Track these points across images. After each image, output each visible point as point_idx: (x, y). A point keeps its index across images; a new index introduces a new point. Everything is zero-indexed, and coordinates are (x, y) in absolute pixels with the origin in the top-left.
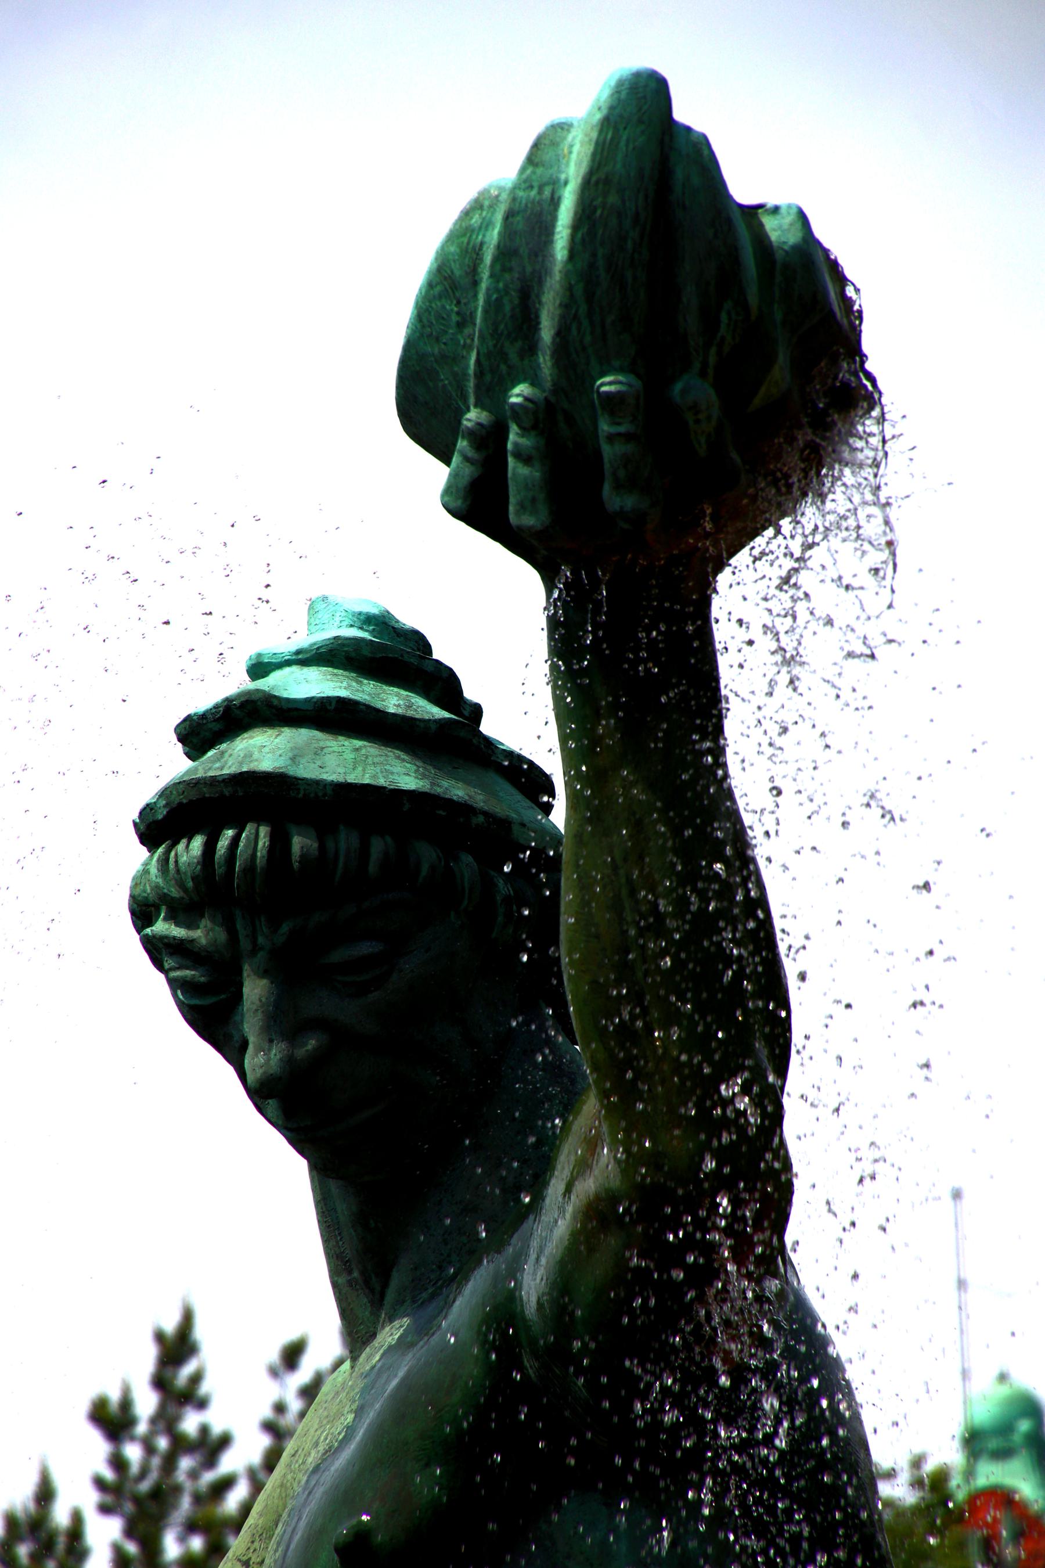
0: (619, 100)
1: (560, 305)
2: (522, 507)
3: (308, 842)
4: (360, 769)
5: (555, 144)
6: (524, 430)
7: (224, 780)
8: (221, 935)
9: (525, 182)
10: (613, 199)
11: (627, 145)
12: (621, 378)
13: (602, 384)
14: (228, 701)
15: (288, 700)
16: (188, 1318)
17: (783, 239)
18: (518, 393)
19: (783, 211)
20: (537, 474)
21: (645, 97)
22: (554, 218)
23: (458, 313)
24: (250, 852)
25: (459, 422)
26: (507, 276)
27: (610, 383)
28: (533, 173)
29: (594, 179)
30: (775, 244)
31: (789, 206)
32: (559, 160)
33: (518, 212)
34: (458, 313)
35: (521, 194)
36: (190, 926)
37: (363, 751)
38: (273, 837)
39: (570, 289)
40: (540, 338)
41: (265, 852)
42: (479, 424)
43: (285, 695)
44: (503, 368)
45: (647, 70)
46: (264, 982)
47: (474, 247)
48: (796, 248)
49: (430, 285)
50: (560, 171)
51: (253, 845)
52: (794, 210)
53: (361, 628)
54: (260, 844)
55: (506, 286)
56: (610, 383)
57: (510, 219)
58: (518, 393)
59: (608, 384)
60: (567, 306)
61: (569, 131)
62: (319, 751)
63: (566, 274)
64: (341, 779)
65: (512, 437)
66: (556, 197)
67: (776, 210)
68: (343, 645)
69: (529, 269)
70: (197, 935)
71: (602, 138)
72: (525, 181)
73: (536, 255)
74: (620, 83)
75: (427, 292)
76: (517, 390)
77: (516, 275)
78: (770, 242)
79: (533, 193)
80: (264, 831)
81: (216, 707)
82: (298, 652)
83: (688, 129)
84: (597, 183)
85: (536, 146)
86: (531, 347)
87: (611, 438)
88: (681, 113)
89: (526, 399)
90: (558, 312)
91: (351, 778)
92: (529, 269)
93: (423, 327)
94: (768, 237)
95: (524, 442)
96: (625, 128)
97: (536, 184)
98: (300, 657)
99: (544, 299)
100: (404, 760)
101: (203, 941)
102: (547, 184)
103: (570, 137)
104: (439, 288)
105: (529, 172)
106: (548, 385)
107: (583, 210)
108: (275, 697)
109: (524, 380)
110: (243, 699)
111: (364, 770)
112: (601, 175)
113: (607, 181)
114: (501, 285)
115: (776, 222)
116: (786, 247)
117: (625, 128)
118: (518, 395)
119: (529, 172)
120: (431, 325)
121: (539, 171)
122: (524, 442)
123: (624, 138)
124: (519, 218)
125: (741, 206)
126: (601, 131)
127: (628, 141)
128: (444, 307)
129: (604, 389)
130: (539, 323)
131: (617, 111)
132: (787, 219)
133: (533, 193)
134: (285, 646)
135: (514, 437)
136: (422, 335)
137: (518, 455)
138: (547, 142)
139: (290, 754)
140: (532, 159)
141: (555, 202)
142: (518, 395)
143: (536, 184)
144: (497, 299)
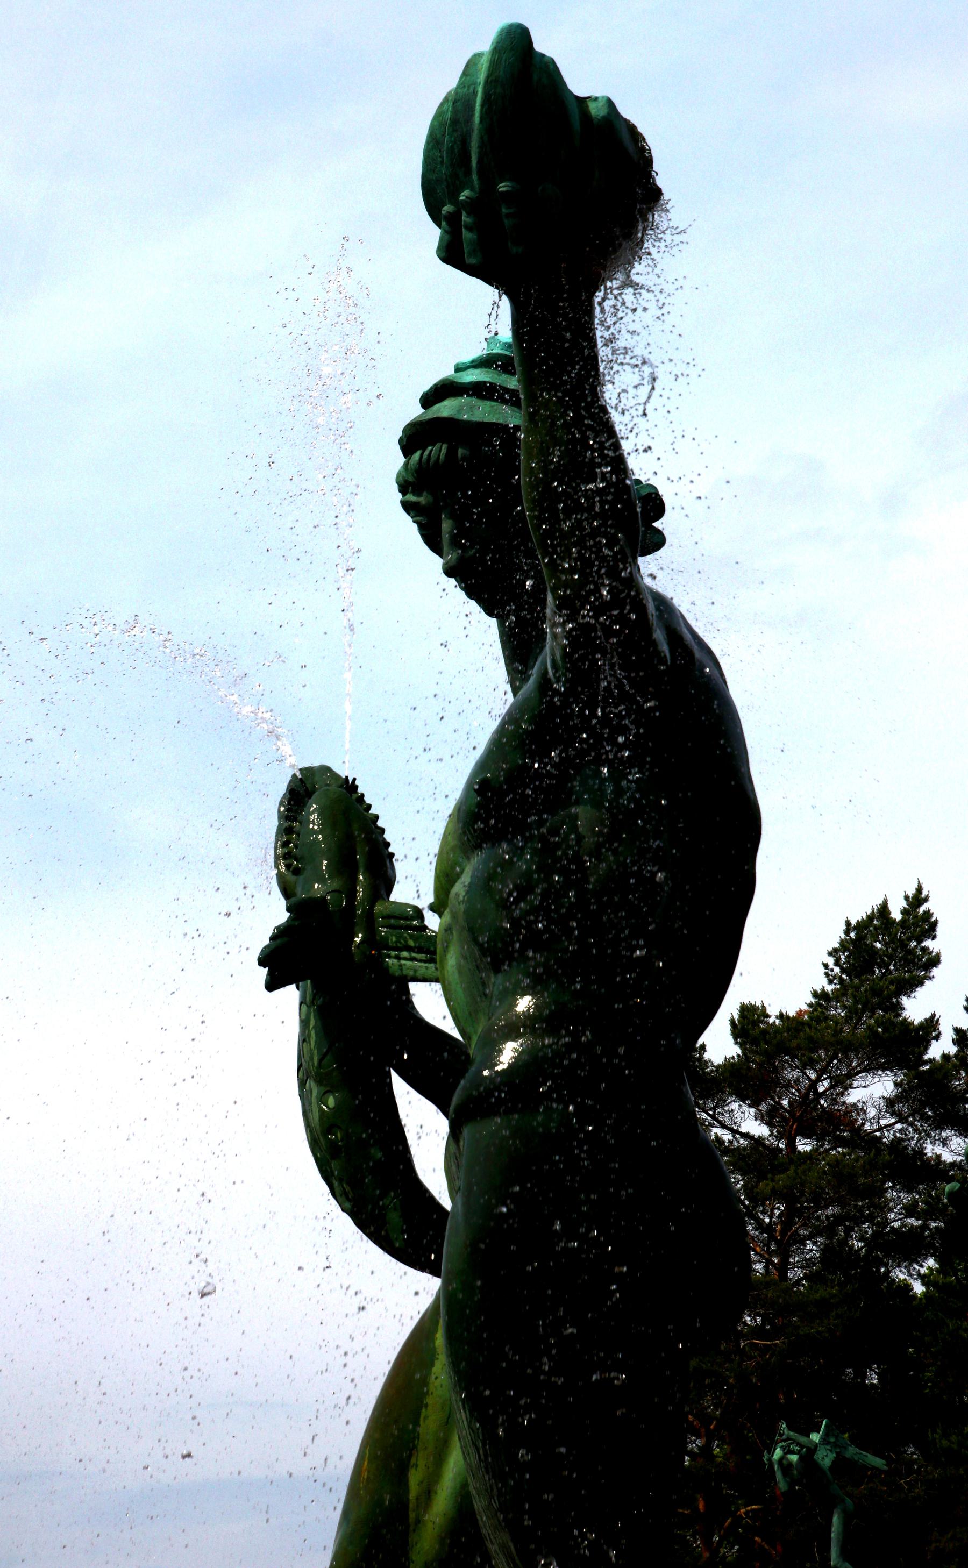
0: (502, 39)
1: (478, 147)
2: (470, 255)
3: (465, 451)
4: (491, 415)
5: (475, 64)
6: (469, 214)
7: (426, 422)
8: (431, 499)
9: (461, 84)
10: (499, 90)
11: (505, 63)
12: (508, 184)
13: (500, 188)
14: (435, 385)
15: (461, 383)
16: (919, 890)
17: (597, 114)
18: (464, 195)
19: (600, 100)
20: (475, 237)
21: (514, 37)
22: (475, 102)
23: (440, 157)
24: (436, 456)
25: (441, 213)
26: (455, 134)
27: (503, 187)
28: (465, 80)
29: (489, 80)
30: (593, 116)
31: (603, 97)
32: (477, 71)
33: (459, 100)
34: (440, 157)
35: (460, 90)
36: (419, 495)
37: (495, 407)
38: (448, 449)
39: (481, 138)
40: (472, 166)
41: (444, 456)
42: (448, 212)
43: (460, 381)
44: (458, 182)
45: (517, 23)
46: (451, 521)
47: (445, 122)
48: (604, 117)
49: (428, 143)
50: (477, 78)
51: (438, 453)
52: (605, 99)
53: (506, 350)
54: (442, 452)
55: (455, 139)
56: (503, 187)
57: (455, 104)
58: (464, 195)
59: (503, 187)
60: (481, 146)
61: (482, 57)
62: (471, 408)
63: (480, 130)
64: (481, 420)
65: (463, 218)
66: (476, 90)
67: (596, 99)
68: (492, 357)
69: (465, 130)
70: (422, 500)
71: (493, 58)
72: (462, 84)
73: (468, 122)
74: (502, 30)
75: (427, 147)
76: (463, 194)
77: (459, 133)
78: (591, 115)
79: (465, 90)
80: (445, 446)
81: (431, 388)
82: (473, 361)
83: (543, 56)
84: (491, 82)
85: (467, 66)
86: (468, 172)
87: (508, 216)
88: (539, 46)
89: (467, 197)
90: (477, 150)
91: (486, 420)
92: (465, 130)
93: (427, 165)
94: (590, 113)
95: (468, 220)
96: (504, 53)
97: (466, 85)
98: (474, 364)
99: (472, 145)
100: (516, 411)
101: (424, 502)
102: (471, 85)
103: (482, 60)
104: (431, 144)
105: (463, 79)
106: (477, 190)
107: (485, 96)
108: (455, 382)
109: (467, 189)
110: (441, 384)
111: (493, 416)
112: (493, 78)
113: (496, 81)
114: (453, 139)
115: (595, 105)
116: (599, 118)
117: (504, 53)
118: (463, 196)
119: (463, 79)
120: (430, 164)
121: (468, 78)
122: (468, 220)
123: (504, 58)
124: (458, 104)
125: (577, 98)
126: (492, 55)
127: (506, 60)
128: (434, 154)
129: (501, 190)
130: (471, 158)
131: (501, 44)
132: (601, 103)
133: (465, 90)
134: (467, 358)
135: (465, 218)
136: (427, 170)
137: (466, 228)
138: (472, 63)
139: (457, 409)
140: (465, 73)
141: (475, 94)
142: (463, 196)
143: (466, 85)
144: (451, 146)
